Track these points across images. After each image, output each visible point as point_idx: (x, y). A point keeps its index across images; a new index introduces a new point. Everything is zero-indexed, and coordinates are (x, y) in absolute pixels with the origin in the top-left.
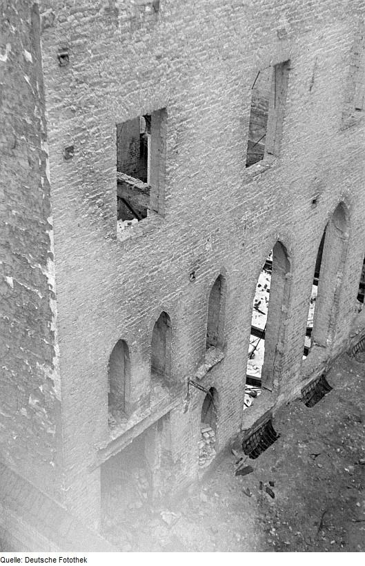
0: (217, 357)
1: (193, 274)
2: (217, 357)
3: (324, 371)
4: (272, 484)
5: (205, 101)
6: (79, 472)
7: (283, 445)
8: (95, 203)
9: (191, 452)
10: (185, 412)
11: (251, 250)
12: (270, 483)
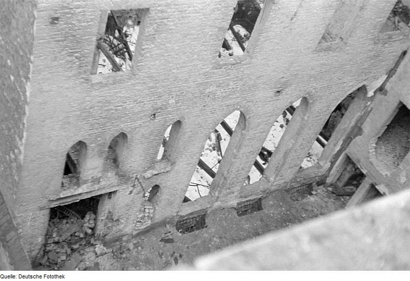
0: (165, 168)
1: (154, 115)
2: (165, 168)
3: (262, 197)
4: (181, 256)
5: (187, 11)
6: (30, 208)
8: (72, 55)
9: (130, 217)
10: (129, 194)
11: (211, 111)
12: (180, 255)
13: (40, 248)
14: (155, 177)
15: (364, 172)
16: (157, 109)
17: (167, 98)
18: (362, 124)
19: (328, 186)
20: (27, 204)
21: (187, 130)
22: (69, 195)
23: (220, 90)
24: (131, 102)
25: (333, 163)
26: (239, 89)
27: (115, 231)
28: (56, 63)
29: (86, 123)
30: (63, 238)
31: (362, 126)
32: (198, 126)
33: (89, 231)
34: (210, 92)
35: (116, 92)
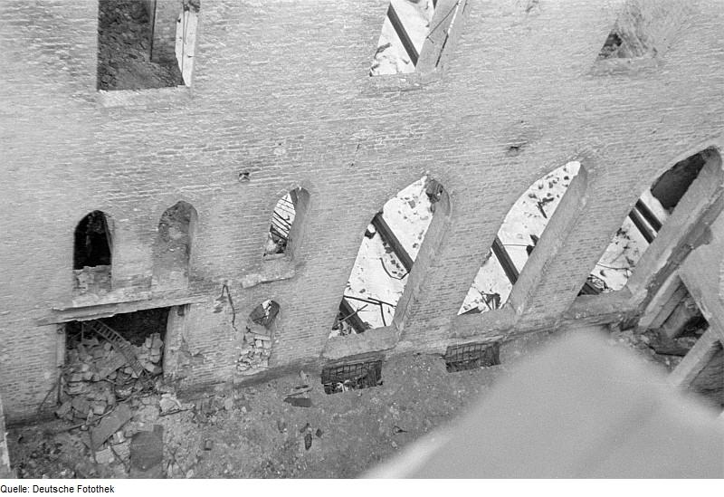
4: (319, 433)
7: (374, 396)
8: (53, 53)
10: (215, 312)
13: (49, 388)
14: (265, 285)
15: (707, 316)
16: (250, 164)
17: (268, 145)
18: (711, 223)
19: (643, 334)
20: (9, 313)
21: (321, 207)
22: (89, 304)
23: (384, 138)
24: (193, 146)
25: (652, 291)
26: (423, 138)
27: (195, 374)
28: (18, 65)
29: (103, 180)
30: (102, 375)
31: (712, 226)
32: (345, 201)
33: (151, 368)
34: (360, 140)
35: (158, 127)
